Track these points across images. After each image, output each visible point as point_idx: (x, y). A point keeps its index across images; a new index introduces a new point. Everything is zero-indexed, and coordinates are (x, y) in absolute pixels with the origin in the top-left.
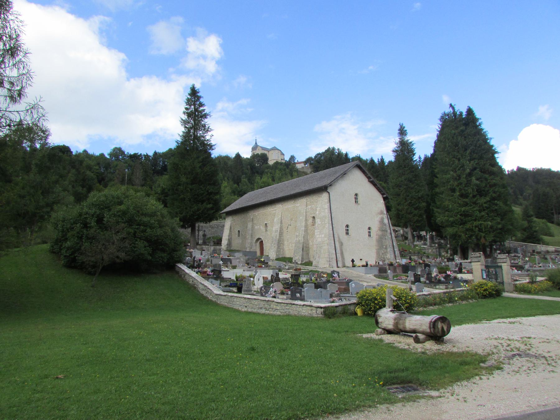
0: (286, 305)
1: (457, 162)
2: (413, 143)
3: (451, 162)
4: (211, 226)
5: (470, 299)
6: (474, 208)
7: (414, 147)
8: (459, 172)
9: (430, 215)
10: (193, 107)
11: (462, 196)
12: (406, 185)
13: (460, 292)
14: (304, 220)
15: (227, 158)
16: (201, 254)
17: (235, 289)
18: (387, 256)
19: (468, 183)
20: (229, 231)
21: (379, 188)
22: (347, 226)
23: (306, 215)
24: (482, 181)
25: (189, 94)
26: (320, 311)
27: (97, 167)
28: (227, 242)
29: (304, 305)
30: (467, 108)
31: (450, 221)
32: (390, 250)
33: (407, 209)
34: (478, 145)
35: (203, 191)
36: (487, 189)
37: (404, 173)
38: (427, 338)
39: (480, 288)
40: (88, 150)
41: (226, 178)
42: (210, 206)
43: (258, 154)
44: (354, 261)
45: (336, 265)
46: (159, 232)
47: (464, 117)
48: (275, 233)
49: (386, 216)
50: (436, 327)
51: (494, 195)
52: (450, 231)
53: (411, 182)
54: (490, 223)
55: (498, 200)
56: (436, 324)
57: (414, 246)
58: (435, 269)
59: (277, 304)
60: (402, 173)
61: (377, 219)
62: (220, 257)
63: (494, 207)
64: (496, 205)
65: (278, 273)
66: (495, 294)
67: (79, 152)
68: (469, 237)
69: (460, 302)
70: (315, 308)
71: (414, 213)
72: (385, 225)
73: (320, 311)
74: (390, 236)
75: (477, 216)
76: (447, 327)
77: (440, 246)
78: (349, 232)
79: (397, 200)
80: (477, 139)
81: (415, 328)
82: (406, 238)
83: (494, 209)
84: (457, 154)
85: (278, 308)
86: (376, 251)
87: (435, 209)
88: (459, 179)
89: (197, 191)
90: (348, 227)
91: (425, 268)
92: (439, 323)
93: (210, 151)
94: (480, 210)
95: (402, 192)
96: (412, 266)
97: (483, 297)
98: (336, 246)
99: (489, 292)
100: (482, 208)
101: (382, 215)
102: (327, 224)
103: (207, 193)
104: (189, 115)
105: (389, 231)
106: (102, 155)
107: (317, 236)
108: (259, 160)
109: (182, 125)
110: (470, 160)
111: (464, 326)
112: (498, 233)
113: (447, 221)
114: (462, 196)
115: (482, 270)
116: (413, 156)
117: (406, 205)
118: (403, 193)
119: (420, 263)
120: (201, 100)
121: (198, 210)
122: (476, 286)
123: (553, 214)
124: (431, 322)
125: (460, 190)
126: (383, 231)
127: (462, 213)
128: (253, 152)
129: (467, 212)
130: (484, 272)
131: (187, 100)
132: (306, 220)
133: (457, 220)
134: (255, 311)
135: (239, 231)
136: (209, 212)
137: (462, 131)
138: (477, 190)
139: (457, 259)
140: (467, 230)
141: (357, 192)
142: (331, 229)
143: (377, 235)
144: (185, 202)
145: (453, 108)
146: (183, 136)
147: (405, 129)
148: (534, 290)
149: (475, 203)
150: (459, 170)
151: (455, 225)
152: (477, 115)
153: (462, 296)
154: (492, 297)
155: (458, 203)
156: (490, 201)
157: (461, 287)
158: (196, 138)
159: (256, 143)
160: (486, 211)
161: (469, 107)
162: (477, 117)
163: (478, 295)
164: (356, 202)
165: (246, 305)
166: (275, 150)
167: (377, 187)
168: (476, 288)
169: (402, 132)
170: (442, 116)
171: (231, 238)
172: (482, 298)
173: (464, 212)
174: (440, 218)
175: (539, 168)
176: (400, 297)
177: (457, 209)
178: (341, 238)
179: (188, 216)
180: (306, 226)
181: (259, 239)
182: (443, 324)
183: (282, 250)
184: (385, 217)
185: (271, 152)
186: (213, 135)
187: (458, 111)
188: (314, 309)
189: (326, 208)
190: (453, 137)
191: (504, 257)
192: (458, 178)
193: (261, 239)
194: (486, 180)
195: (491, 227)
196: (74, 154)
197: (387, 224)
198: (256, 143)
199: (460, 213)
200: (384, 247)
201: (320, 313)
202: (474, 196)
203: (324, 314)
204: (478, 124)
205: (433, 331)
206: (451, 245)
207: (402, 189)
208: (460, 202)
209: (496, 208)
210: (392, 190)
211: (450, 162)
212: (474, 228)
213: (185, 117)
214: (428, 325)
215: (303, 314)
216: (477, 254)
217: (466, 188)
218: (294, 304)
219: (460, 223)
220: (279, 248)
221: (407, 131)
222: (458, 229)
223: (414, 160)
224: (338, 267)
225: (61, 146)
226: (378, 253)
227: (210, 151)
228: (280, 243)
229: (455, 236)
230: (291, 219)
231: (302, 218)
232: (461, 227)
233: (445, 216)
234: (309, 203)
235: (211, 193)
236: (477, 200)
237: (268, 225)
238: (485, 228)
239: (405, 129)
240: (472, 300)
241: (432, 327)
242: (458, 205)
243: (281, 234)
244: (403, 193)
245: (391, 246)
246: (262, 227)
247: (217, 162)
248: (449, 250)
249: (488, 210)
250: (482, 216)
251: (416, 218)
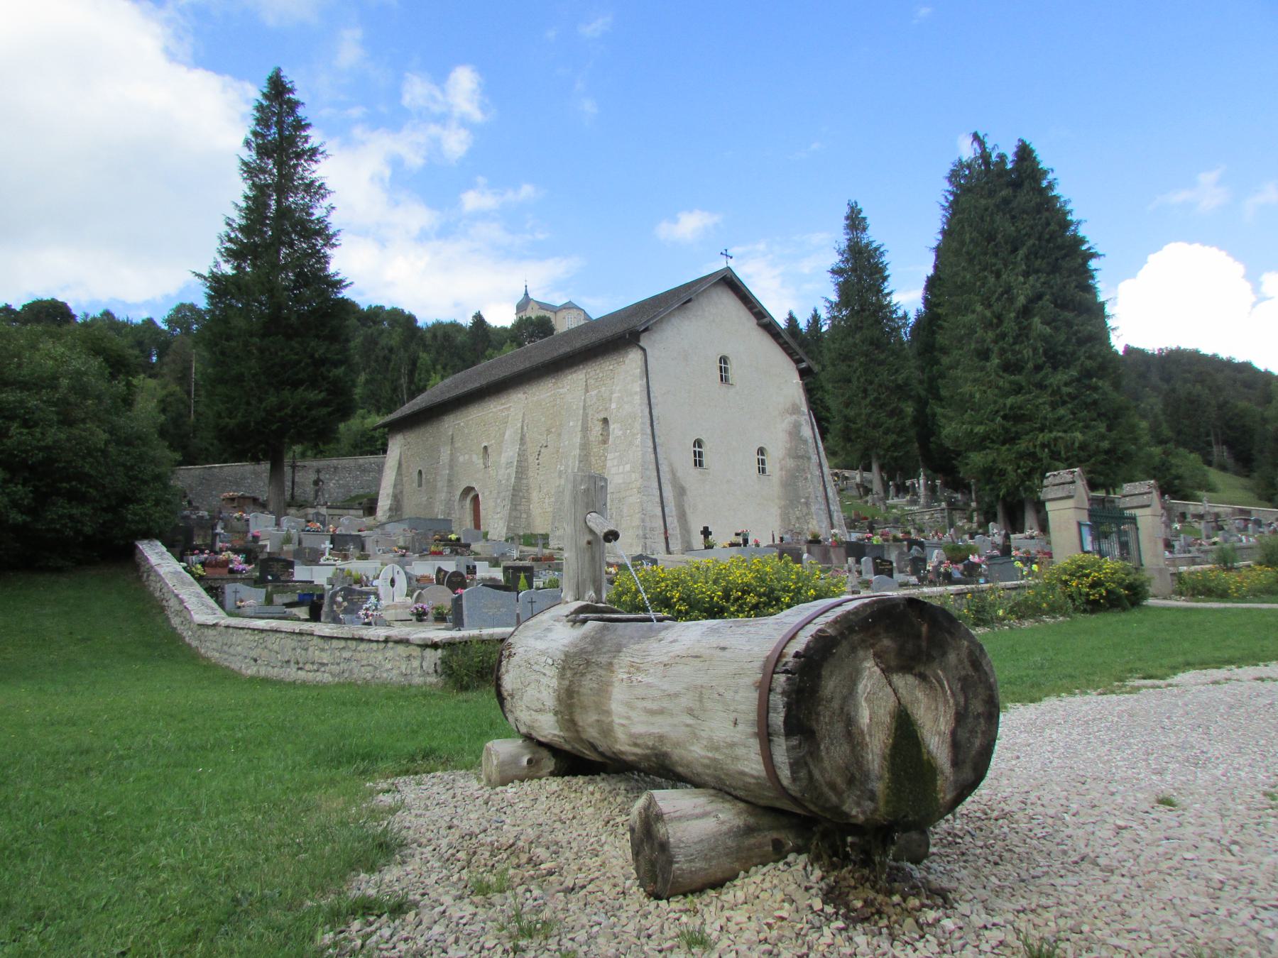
0: (342, 644)
1: (992, 280)
2: (882, 250)
3: (978, 283)
4: (360, 466)
5: (1047, 613)
6: (1037, 397)
7: (885, 259)
8: (997, 307)
9: (926, 428)
10: (274, 130)
11: (1007, 367)
12: (867, 356)
13: (1014, 593)
14: (580, 428)
15: (455, 326)
16: (278, 524)
17: (303, 612)
18: (810, 526)
19: (1023, 334)
20: (394, 473)
21: (786, 343)
22: (698, 443)
23: (585, 416)
24: (1056, 329)
25: (265, 95)
26: (434, 656)
27: (136, 352)
28: (389, 502)
29: (386, 641)
30: (1016, 143)
31: (976, 434)
32: (817, 507)
33: (870, 415)
34: (1047, 236)
35: (297, 354)
36: (1070, 349)
37: (860, 325)
38: (749, 831)
39: (1079, 578)
40: (113, 310)
41: (439, 367)
42: (314, 396)
43: (530, 318)
44: (710, 533)
45: (664, 548)
46: (55, 435)
47: (1009, 166)
48: (507, 468)
49: (807, 417)
50: (826, 723)
51: (1089, 363)
52: (977, 459)
53: (878, 347)
54: (1078, 435)
55: (1100, 378)
56: (831, 685)
57: (887, 508)
58: (936, 551)
59: (320, 642)
60: (856, 325)
61: (786, 423)
62: (328, 531)
63: (1089, 395)
64: (1095, 389)
65: (475, 567)
66: (1127, 596)
67: (91, 315)
68: (1025, 473)
69: (1014, 621)
70: (419, 649)
71: (886, 425)
72: (805, 442)
73: (434, 656)
74: (818, 473)
75: (1045, 418)
76: (960, 717)
77: (952, 506)
78: (704, 459)
79: (843, 395)
80: (1043, 219)
81: (661, 738)
82: (868, 491)
83: (1089, 400)
84: (993, 261)
85: (325, 658)
86: (779, 511)
87: (939, 410)
88: (998, 326)
89: (280, 354)
90: (700, 446)
91: (910, 548)
92: (870, 675)
93: (328, 251)
94: (1052, 402)
95: (855, 372)
96: (874, 545)
97: (1088, 608)
98: (664, 495)
99: (1108, 591)
100: (1058, 398)
101: (794, 417)
102: (639, 436)
103: (309, 361)
104: (263, 151)
105: (814, 458)
106: (150, 322)
107: (614, 470)
108: (533, 332)
109: (245, 179)
110: (1026, 274)
111: (1050, 703)
112: (1102, 463)
113: (970, 433)
114: (1007, 367)
115: (1080, 525)
116: (883, 283)
117: (866, 406)
118: (858, 374)
119: (896, 539)
120: (301, 112)
121: (281, 407)
122: (1065, 571)
123: (1209, 444)
124: (774, 664)
125: (1003, 351)
126: (797, 457)
127: (1007, 412)
128: (520, 315)
129: (1020, 408)
130: (1085, 531)
131: (258, 111)
132: (585, 429)
133: (995, 431)
134: (274, 673)
135: (420, 472)
136: (313, 412)
137: (1006, 201)
138: (1045, 353)
139: (995, 531)
140: (1021, 456)
141: (725, 353)
142: (651, 450)
143: (781, 469)
144: (245, 384)
146: (248, 208)
147: (862, 215)
148: (1238, 589)
149: (1041, 386)
150: (998, 299)
151: (991, 445)
152: (1045, 159)
153: (1018, 604)
154: (1116, 606)
155: (998, 387)
156: (1078, 380)
157: (1015, 574)
158: (284, 213)
159: (526, 294)
160: (1070, 406)
162: (1043, 165)
163: (1073, 600)
164: (724, 379)
165: (254, 654)
166: (570, 308)
167: (781, 341)
168: (1064, 577)
169: (855, 221)
170: (952, 171)
171: (401, 492)
172: (1085, 611)
173: (1011, 408)
174: (951, 429)
175: (1174, 347)
176: (772, 590)
177: (995, 402)
178: (679, 474)
179: (252, 424)
180: (585, 446)
181: (469, 490)
182: (904, 682)
183: (524, 516)
184: (804, 423)
185: (560, 315)
186: (333, 208)
187: (993, 149)
188: (416, 652)
189: (636, 393)
190: (982, 219)
191: (1143, 490)
192: (995, 321)
193: (472, 489)
194: (1069, 324)
195: (1083, 447)
196: (79, 320)
197: (811, 441)
198: (526, 294)
199: (1002, 413)
200: (803, 500)
201: (431, 670)
202: (1038, 368)
203: (444, 673)
204: (1044, 184)
205: (795, 766)
206: (978, 503)
207: (856, 364)
208: (1001, 384)
209: (1096, 396)
210: (830, 368)
211: (975, 284)
212: (1038, 449)
213: (250, 156)
214: (747, 701)
215: (385, 675)
216: (1064, 475)
217: (1017, 347)
218: (361, 640)
219: (1001, 438)
220: (516, 510)
221: (868, 221)
222: (999, 454)
224: (668, 552)
225: (47, 301)
226: (785, 517)
227: (328, 251)
228: (518, 496)
229: (990, 474)
230: (549, 431)
231: (574, 424)
232: (1004, 448)
233: (963, 423)
234: (593, 382)
235: (323, 362)
236: (1046, 376)
237: (489, 450)
238: (1068, 449)
239: (862, 215)
240: (1054, 618)
241: (778, 719)
242: (996, 391)
243: (522, 471)
244: (858, 374)
245: (821, 500)
246: (475, 458)
247: (429, 335)
248: (975, 514)
249: (1076, 402)
250: (1059, 419)
251: (892, 438)
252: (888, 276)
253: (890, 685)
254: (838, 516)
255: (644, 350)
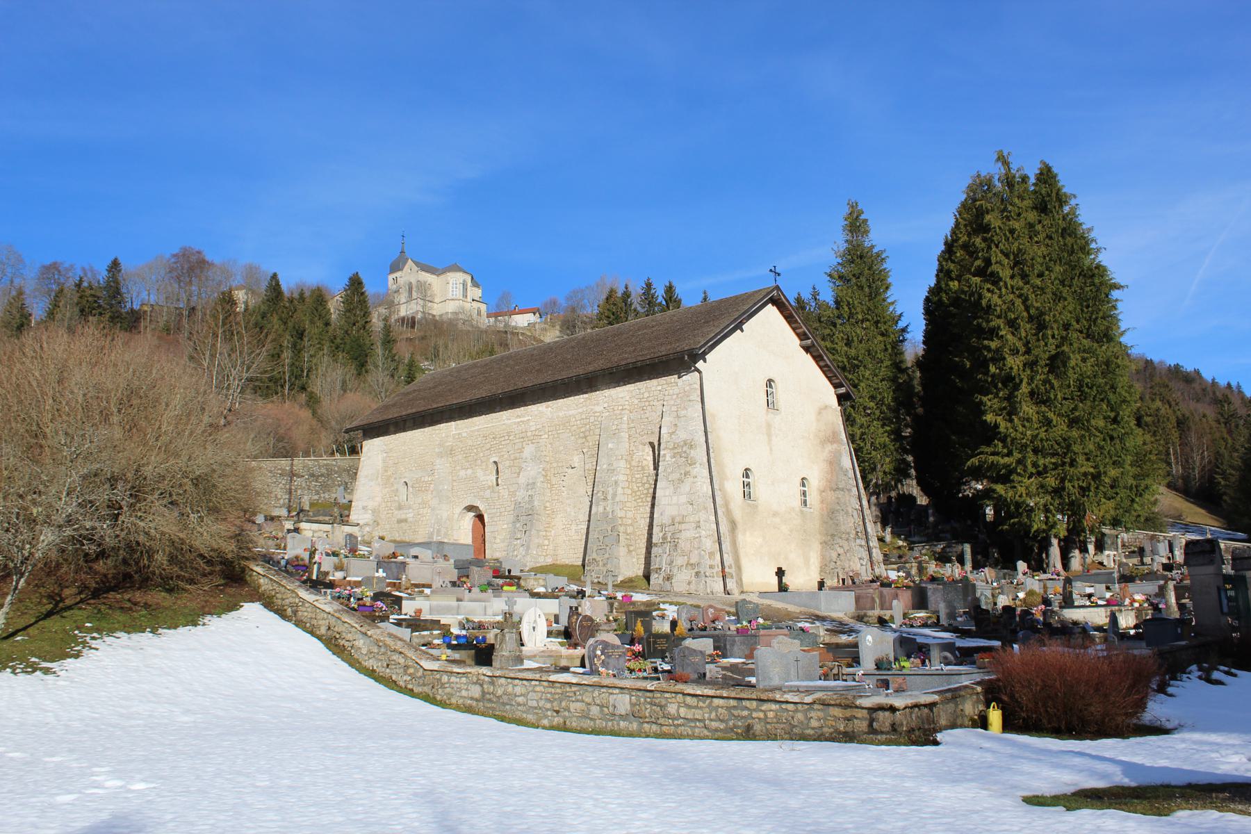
21: (827, 366)
90: (748, 476)
101: (835, 446)
145: (1006, 163)
152: (1066, 183)
161: (1043, 162)
167: (822, 364)
169: (856, 225)
223: (889, 300)
252: (1213, 380)
253: (829, 705)
254: (877, 555)
255: (700, 372)
